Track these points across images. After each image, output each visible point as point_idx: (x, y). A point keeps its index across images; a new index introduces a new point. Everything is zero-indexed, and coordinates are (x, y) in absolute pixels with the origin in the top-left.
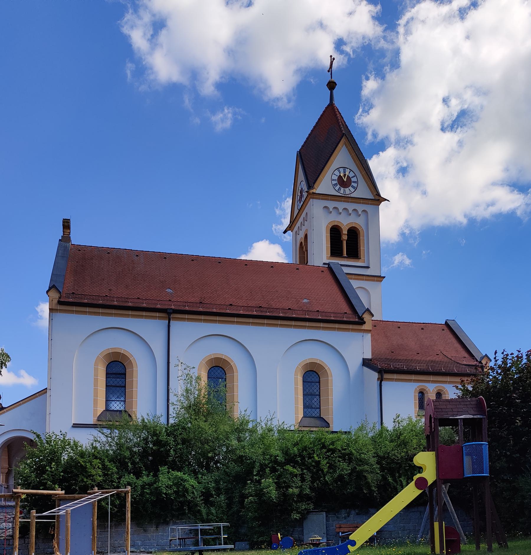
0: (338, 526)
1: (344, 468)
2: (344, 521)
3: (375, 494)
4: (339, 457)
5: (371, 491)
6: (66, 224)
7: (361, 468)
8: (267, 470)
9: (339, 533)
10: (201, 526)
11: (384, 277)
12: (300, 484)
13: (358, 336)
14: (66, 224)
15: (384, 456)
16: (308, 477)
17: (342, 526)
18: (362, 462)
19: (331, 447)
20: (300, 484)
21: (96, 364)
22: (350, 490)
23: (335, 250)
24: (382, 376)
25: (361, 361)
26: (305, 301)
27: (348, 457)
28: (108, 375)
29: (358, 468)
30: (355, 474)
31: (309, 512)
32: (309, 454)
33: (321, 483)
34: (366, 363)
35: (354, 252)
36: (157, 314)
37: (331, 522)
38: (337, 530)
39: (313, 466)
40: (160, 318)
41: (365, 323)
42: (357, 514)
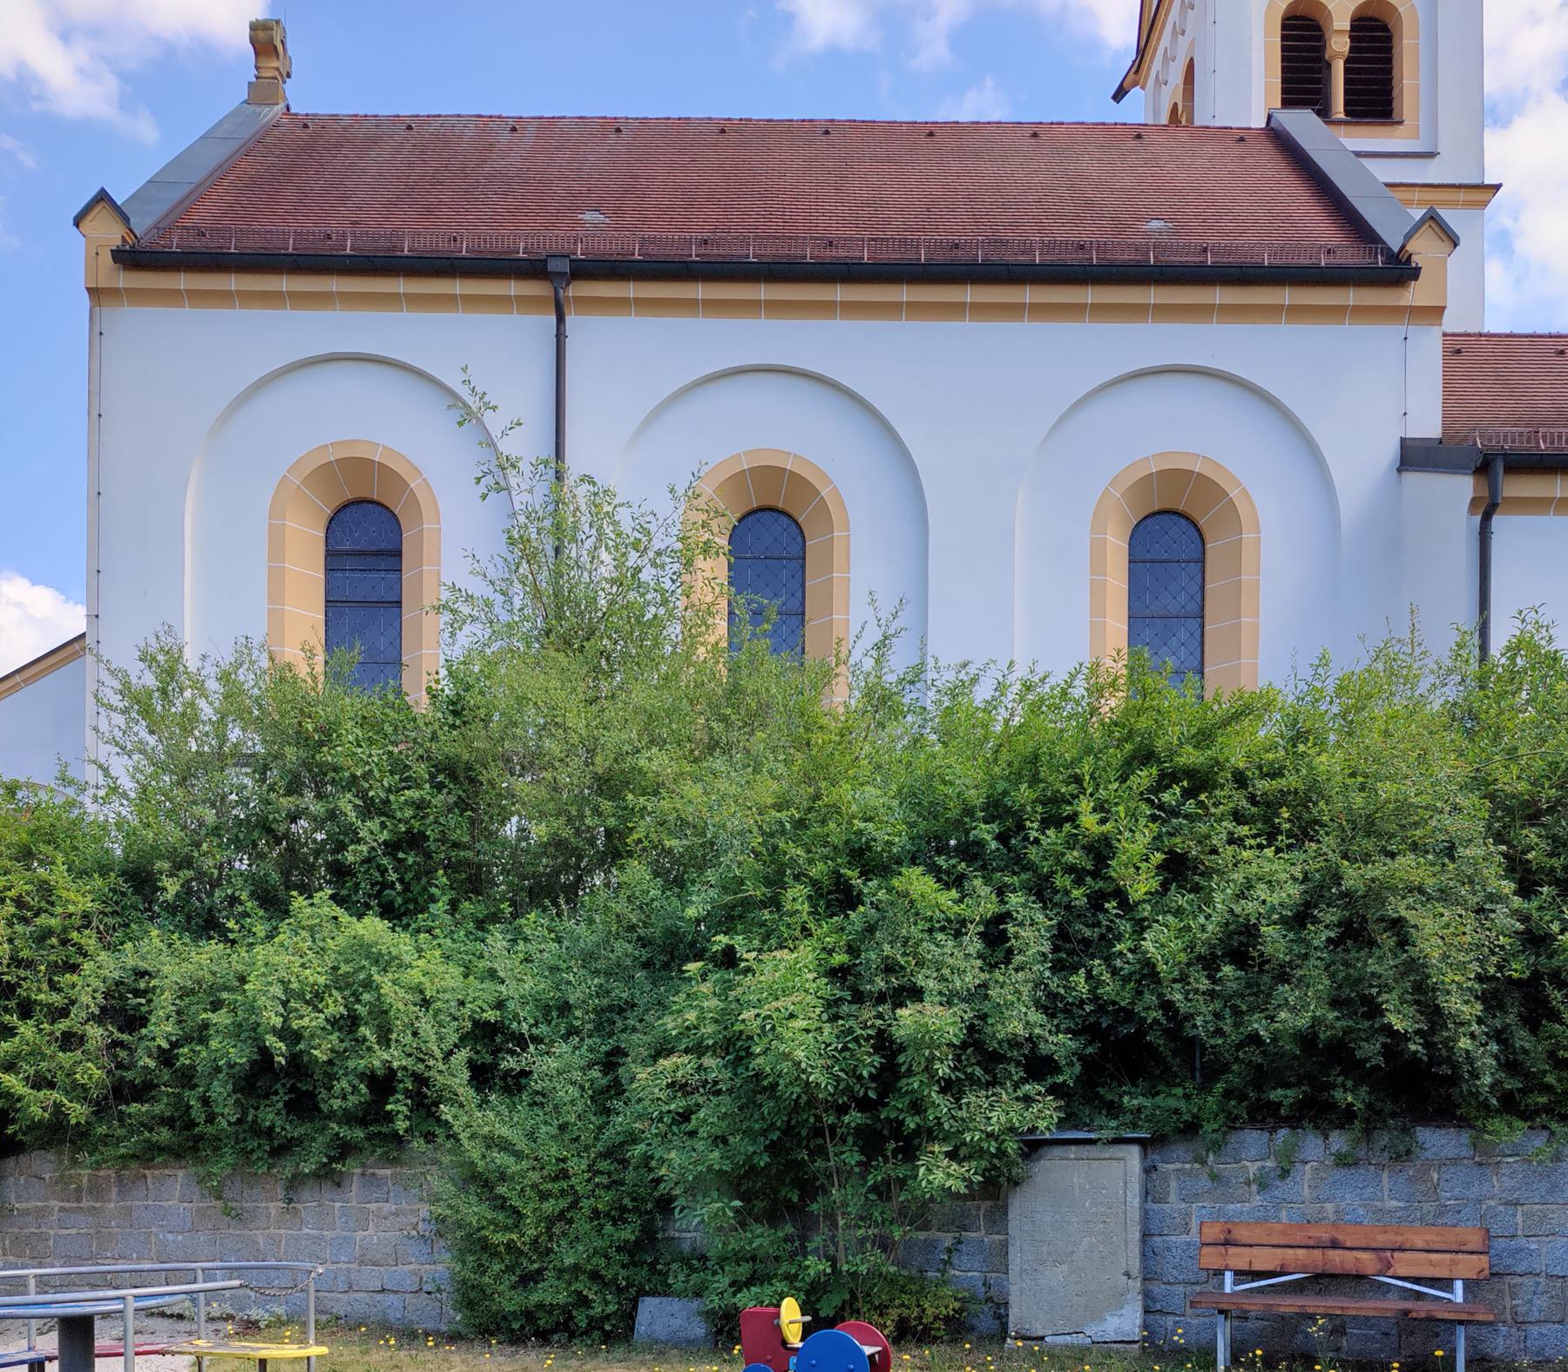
0: (1213, 1232)
1: (1263, 881)
2: (1257, 1200)
3: (1464, 1043)
4: (1238, 817)
5: (1434, 1015)
6: (261, 35)
7: (1371, 871)
8: (796, 897)
9: (1219, 1273)
10: (44, 1284)
11: (1498, 187)
12: (972, 976)
13: (1380, 338)
14: (261, 35)
15: (1533, 802)
16: (1033, 934)
17: (1242, 1234)
18: (1374, 831)
19: (1190, 757)
20: (972, 976)
21: (276, 511)
22: (1299, 1010)
23: (1302, 77)
24: (1494, 489)
25: (1392, 450)
26: (1155, 224)
27: (1281, 815)
28: (335, 559)
29: (1354, 877)
30: (1330, 915)
31: (1033, 1147)
32: (1057, 800)
33: (1115, 972)
34: (1415, 457)
35: (1374, 98)
36: (513, 288)
37: (1174, 1204)
38: (1211, 1258)
39: (1070, 869)
40: (526, 303)
41: (1415, 273)
42: (1343, 1161)
